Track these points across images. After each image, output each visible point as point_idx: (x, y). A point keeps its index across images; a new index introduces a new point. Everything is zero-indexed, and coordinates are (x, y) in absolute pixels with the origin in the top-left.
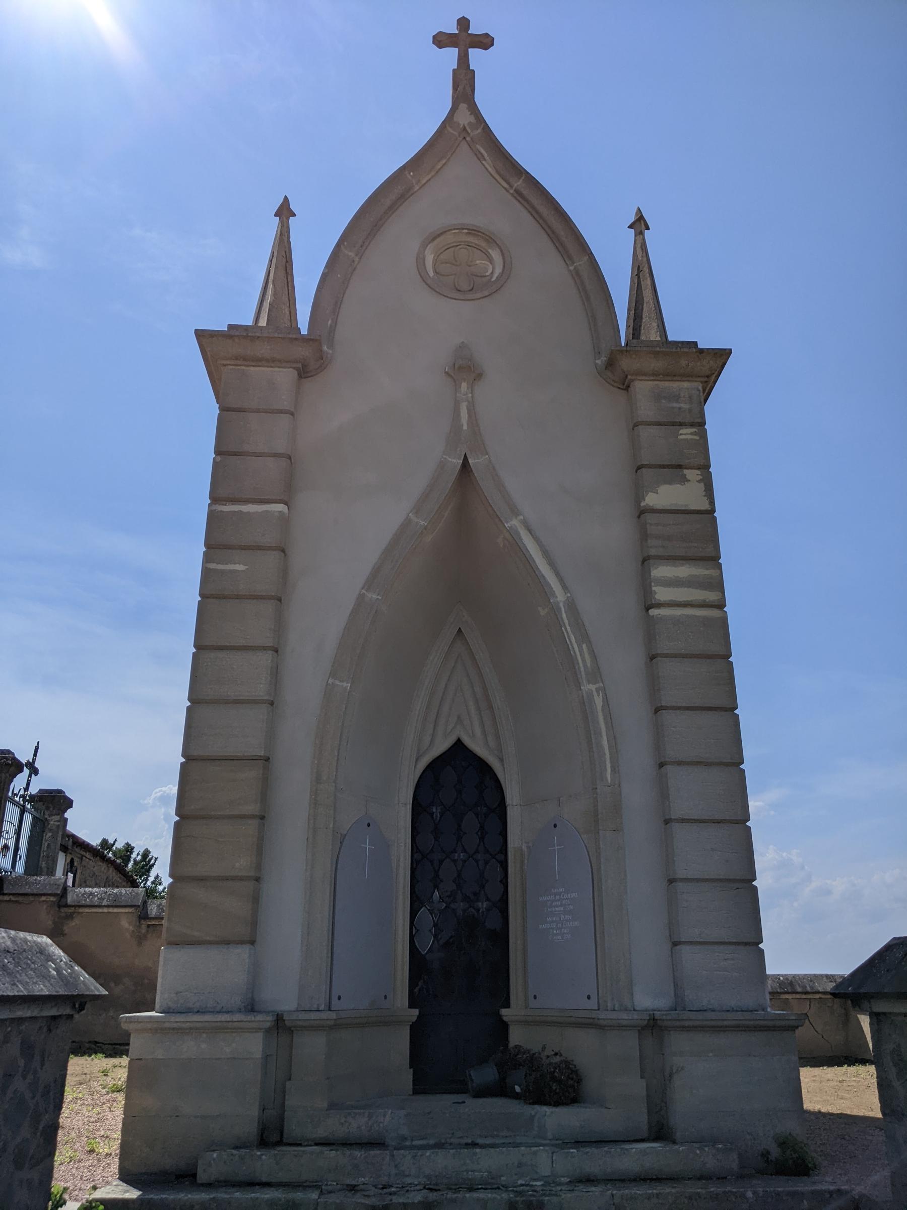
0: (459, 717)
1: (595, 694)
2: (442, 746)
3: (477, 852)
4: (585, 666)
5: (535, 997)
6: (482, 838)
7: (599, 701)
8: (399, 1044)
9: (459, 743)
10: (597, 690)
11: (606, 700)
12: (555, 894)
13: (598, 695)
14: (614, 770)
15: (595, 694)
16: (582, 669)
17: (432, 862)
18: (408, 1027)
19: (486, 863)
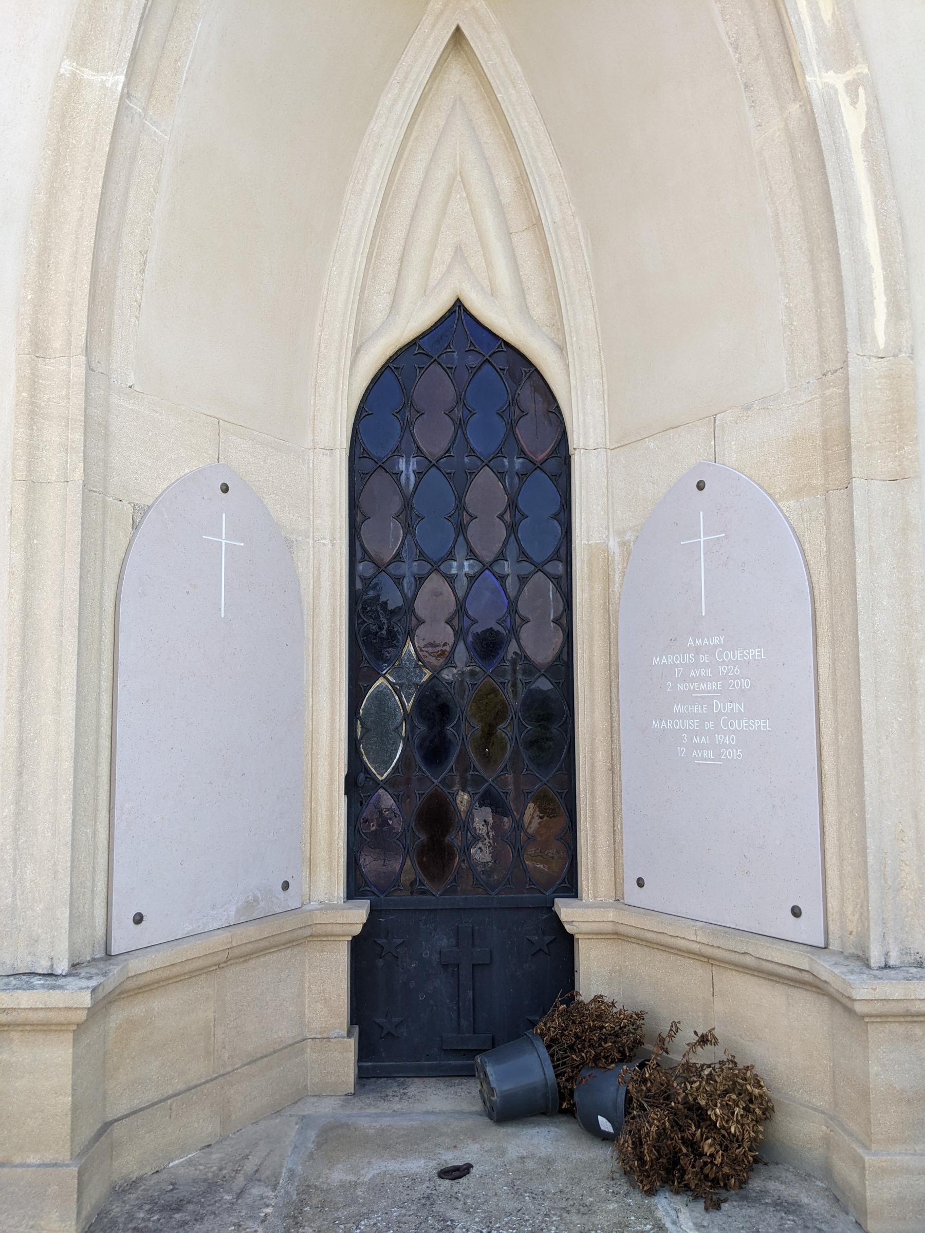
0: (459, 250)
1: (844, 99)
2: (419, 316)
3: (501, 556)
4: (816, 17)
5: (640, 883)
6: (512, 529)
7: (854, 121)
8: (327, 983)
9: (458, 310)
10: (852, 88)
11: (876, 116)
12: (697, 651)
13: (854, 103)
14: (896, 310)
15: (844, 99)
16: (808, 25)
17: (502, 579)
18: (341, 957)
19: (523, 580)
